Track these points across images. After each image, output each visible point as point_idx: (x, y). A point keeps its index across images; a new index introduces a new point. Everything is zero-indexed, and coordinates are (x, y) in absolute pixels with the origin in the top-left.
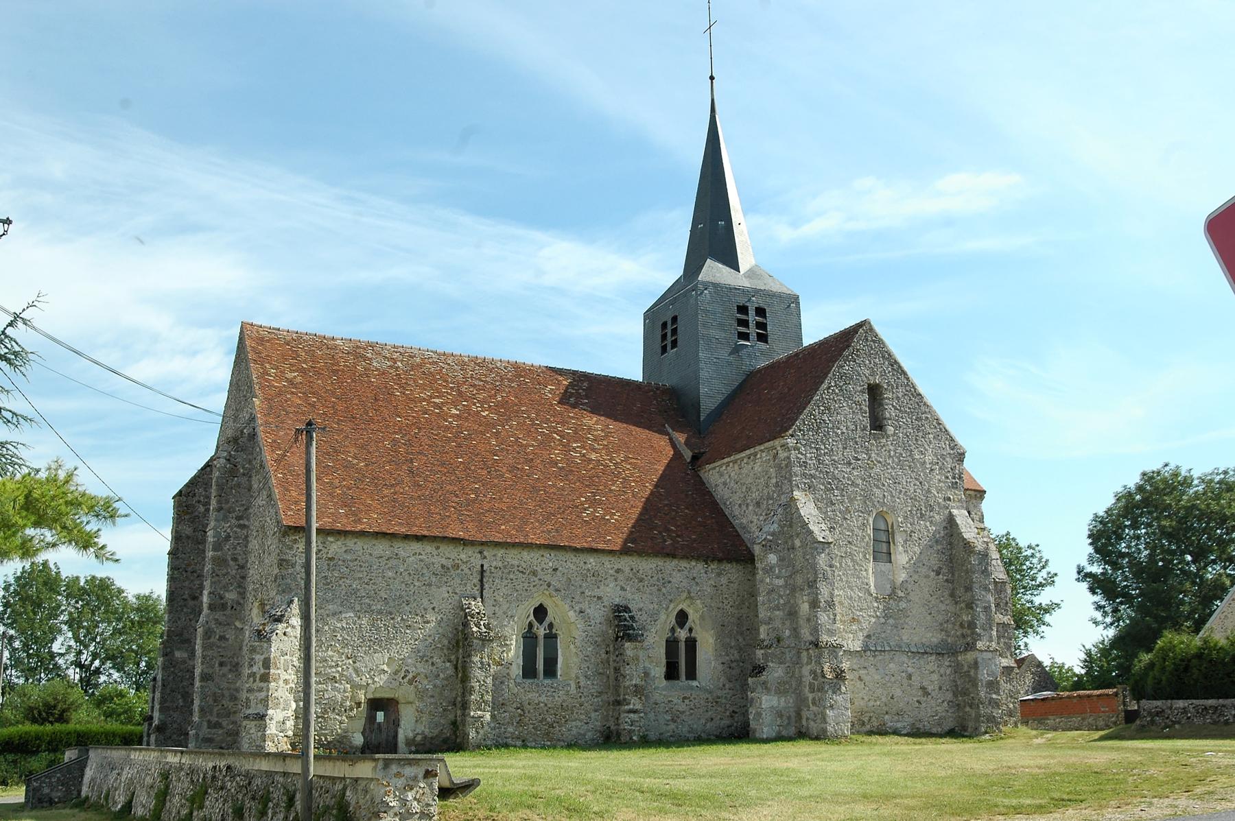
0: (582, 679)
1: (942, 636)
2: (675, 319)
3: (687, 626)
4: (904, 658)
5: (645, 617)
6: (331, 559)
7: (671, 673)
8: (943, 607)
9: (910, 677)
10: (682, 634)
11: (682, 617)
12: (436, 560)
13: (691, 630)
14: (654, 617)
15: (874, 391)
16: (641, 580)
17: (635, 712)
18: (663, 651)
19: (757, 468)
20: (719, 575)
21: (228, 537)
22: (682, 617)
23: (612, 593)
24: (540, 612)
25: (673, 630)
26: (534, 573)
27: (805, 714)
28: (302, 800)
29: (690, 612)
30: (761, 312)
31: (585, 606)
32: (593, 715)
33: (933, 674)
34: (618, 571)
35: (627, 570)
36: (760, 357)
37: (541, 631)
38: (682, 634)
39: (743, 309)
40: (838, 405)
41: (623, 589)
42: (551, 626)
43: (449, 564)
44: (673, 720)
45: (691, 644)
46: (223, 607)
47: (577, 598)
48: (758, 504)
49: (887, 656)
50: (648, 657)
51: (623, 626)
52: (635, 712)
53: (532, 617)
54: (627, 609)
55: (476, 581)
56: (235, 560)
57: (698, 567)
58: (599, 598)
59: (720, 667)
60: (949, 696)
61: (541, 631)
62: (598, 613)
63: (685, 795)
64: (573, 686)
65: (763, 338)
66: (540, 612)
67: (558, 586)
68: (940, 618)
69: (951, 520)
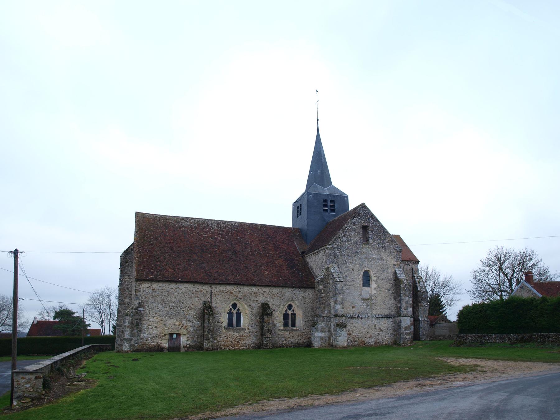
0: (250, 327)
1: (390, 312)
2: (301, 205)
3: (237, 308)
4: (374, 319)
5: (274, 307)
6: (154, 289)
7: (286, 324)
8: (391, 302)
9: (375, 325)
10: (290, 312)
11: (290, 307)
12: (193, 289)
13: (293, 311)
14: (278, 306)
15: (365, 228)
16: (273, 295)
17: (268, 338)
18: (282, 318)
19: (320, 256)
20: (304, 292)
21: (125, 282)
22: (290, 307)
23: (262, 299)
24: (234, 306)
25: (286, 311)
26: (231, 293)
27: (331, 338)
28: (45, 360)
29: (293, 305)
30: (332, 201)
31: (251, 303)
32: (254, 338)
33: (386, 325)
34: (264, 292)
35: (268, 291)
36: (330, 217)
37: (235, 312)
38: (290, 312)
39: (325, 201)
40: (352, 233)
41: (266, 298)
42: (238, 310)
43: (199, 290)
44: (285, 340)
45: (294, 315)
46: (124, 304)
47: (248, 300)
48: (320, 268)
49: (366, 319)
50: (278, 319)
51: (265, 311)
52: (268, 338)
53: (231, 307)
54: (267, 304)
55: (209, 296)
56: (128, 289)
57: (296, 291)
58: (257, 301)
59: (304, 323)
60: (391, 331)
61: (235, 312)
62: (256, 306)
63: (453, 367)
64: (247, 329)
65: (333, 211)
66: (234, 306)
67: (241, 297)
68: (389, 306)
69: (395, 271)
